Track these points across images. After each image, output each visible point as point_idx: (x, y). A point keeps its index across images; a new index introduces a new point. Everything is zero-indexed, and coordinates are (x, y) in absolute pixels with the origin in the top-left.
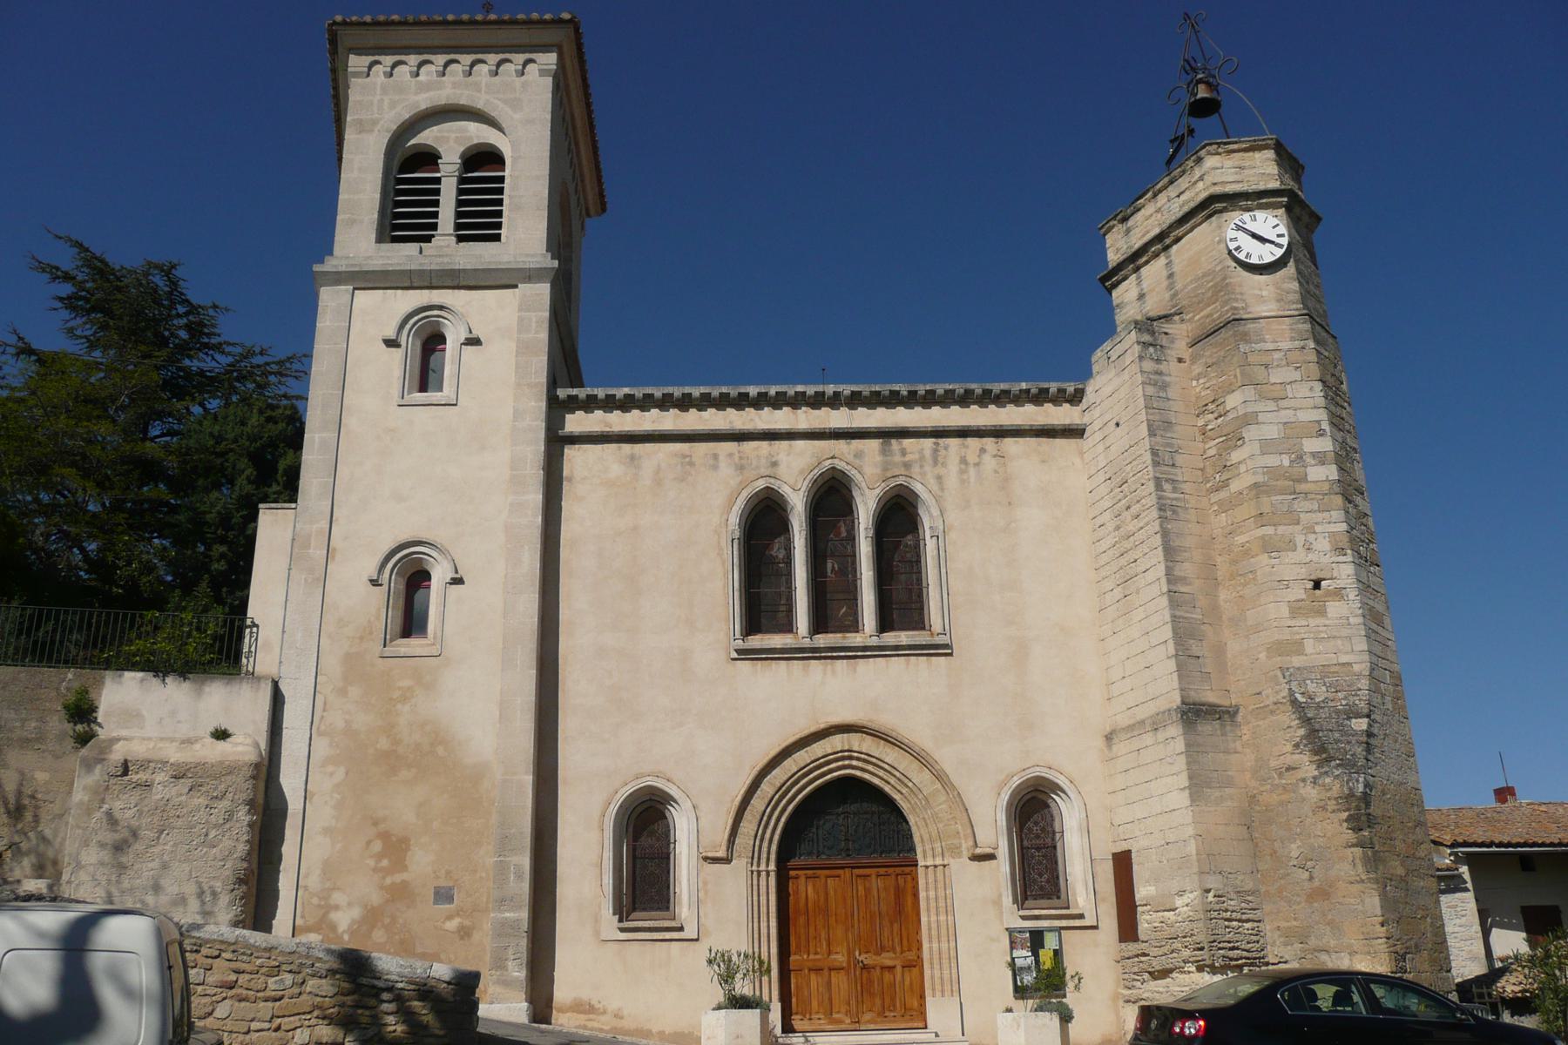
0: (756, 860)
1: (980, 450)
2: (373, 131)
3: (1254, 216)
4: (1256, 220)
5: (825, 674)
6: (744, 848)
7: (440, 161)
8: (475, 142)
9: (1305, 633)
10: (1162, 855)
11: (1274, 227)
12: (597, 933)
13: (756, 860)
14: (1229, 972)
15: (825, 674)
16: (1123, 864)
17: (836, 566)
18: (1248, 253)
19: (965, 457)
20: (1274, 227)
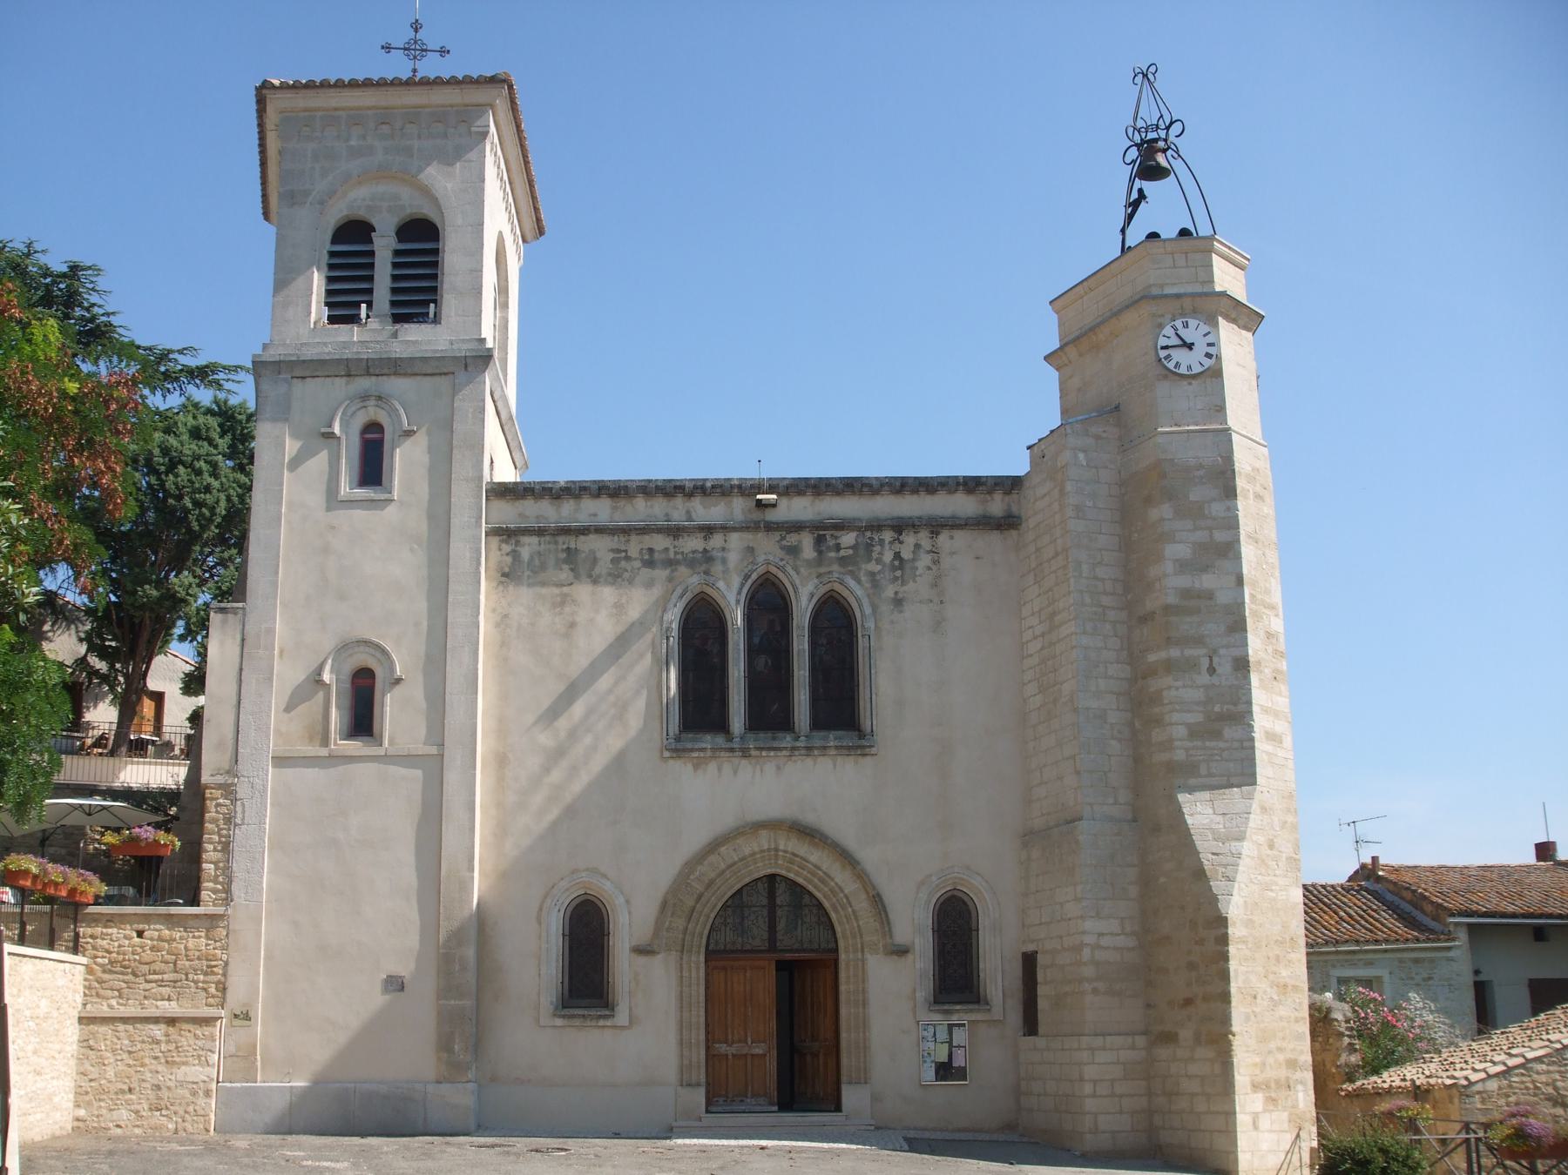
0: (885, 922)
1: (915, 546)
2: (305, 203)
3: (1187, 322)
4: (1187, 327)
5: (754, 772)
6: (674, 942)
7: (373, 234)
8: (408, 211)
9: (1200, 755)
10: (1192, 966)
11: (1205, 335)
12: (538, 1020)
13: (885, 922)
14: (194, 548)
15: (754, 772)
16: (1029, 962)
17: (769, 661)
18: (1177, 363)
19: (899, 552)
20: (1205, 335)
